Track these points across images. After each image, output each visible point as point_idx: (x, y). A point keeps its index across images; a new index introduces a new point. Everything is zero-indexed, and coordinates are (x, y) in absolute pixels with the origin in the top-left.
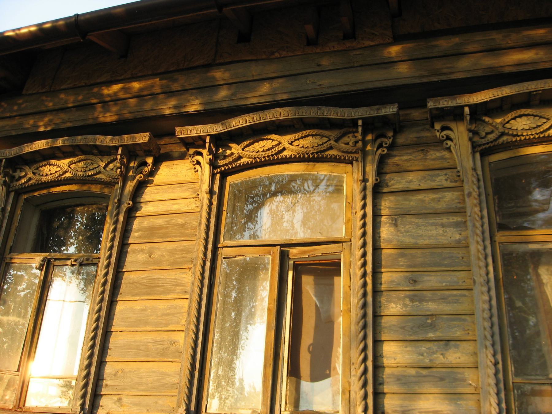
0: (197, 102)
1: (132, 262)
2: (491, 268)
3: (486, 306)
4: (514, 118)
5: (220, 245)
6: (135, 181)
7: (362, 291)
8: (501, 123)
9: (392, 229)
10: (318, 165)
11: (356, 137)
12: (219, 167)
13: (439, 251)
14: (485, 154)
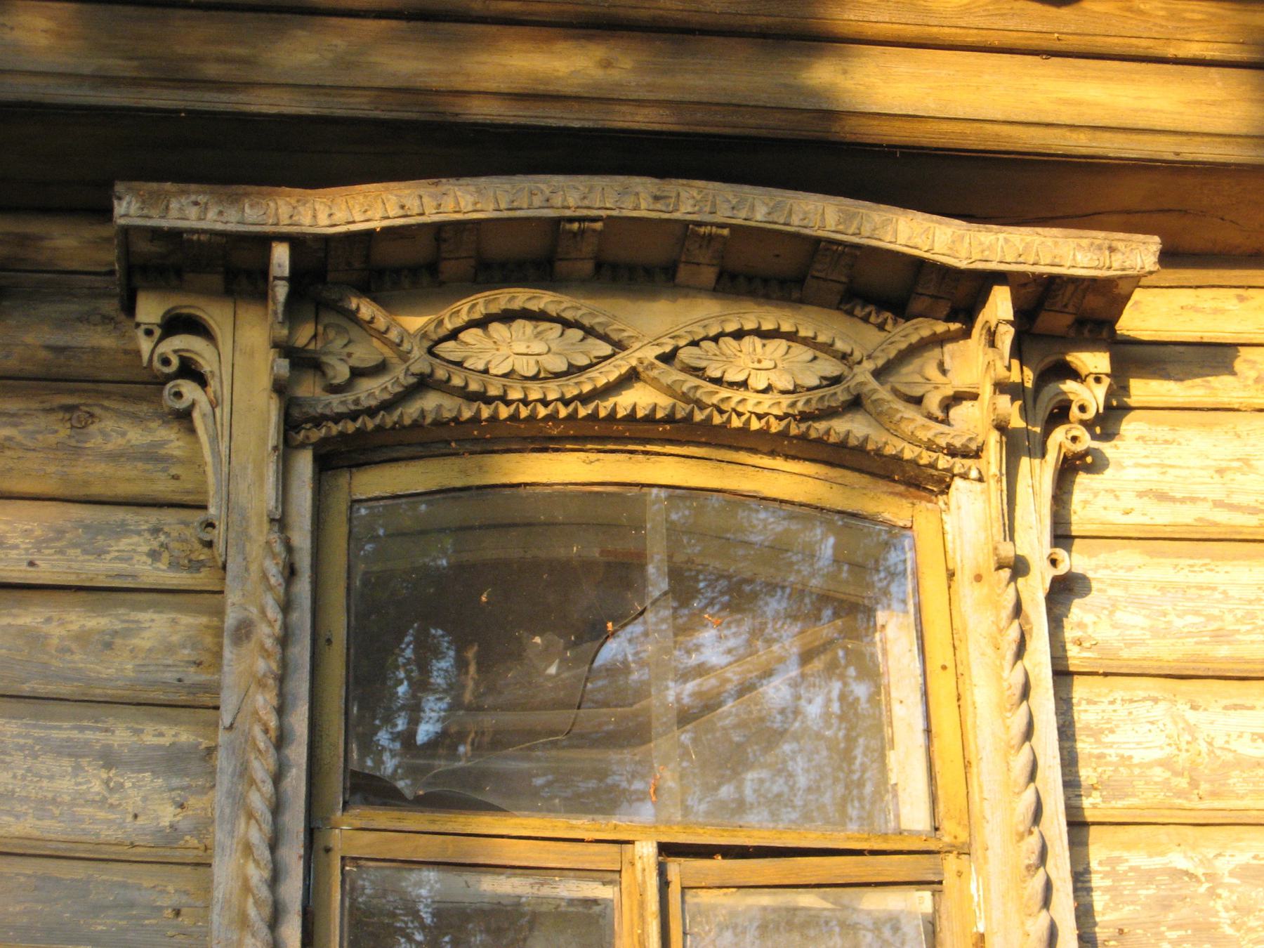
4: (482, 323)
13: (79, 871)
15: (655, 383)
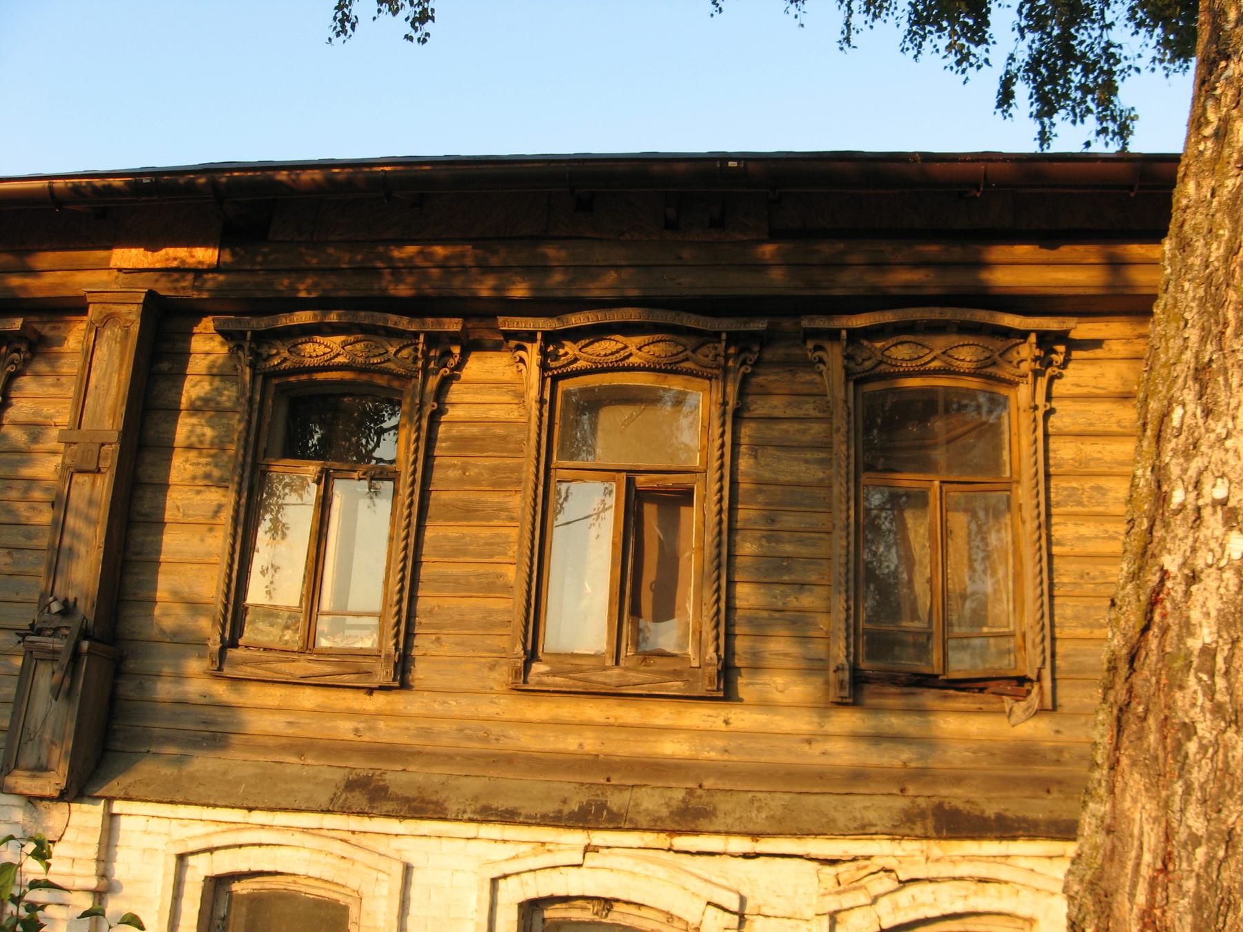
0: (523, 285)
1: (441, 480)
2: (852, 513)
3: (844, 552)
4: (895, 345)
5: (552, 466)
6: (439, 376)
7: (717, 529)
8: (880, 349)
9: (752, 461)
10: (670, 377)
11: (716, 348)
12: (551, 369)
13: (801, 489)
14: (859, 382)
15: (941, 360)
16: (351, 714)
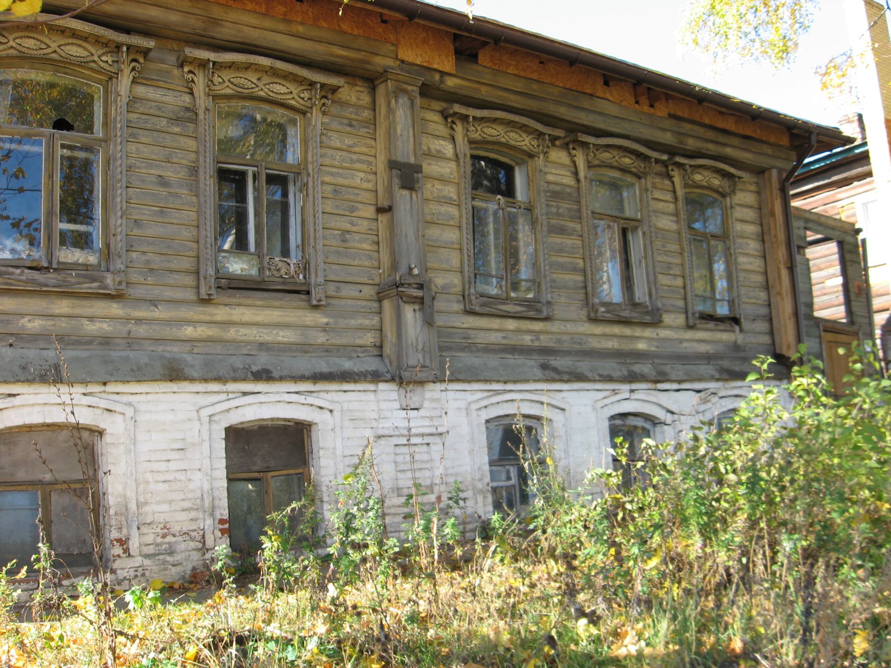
16: (529, 332)
